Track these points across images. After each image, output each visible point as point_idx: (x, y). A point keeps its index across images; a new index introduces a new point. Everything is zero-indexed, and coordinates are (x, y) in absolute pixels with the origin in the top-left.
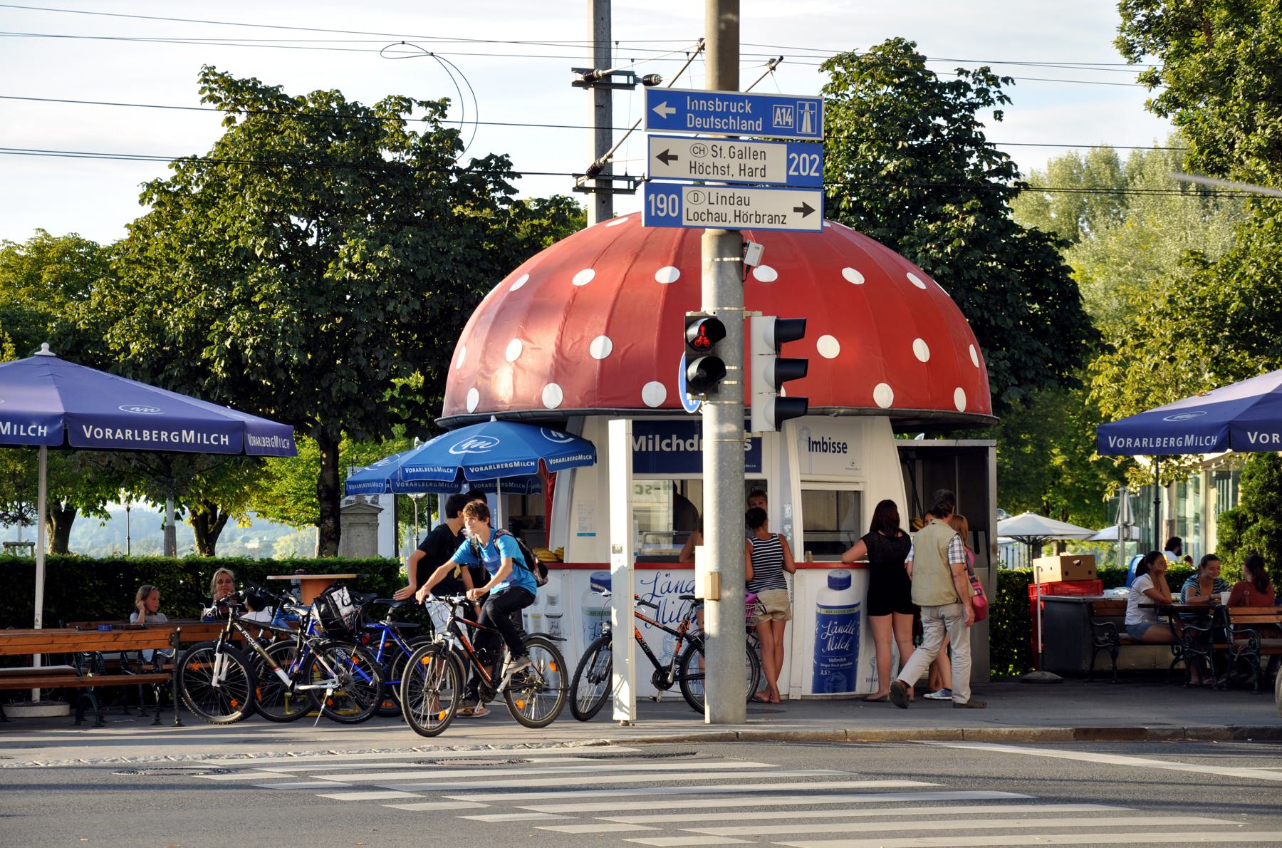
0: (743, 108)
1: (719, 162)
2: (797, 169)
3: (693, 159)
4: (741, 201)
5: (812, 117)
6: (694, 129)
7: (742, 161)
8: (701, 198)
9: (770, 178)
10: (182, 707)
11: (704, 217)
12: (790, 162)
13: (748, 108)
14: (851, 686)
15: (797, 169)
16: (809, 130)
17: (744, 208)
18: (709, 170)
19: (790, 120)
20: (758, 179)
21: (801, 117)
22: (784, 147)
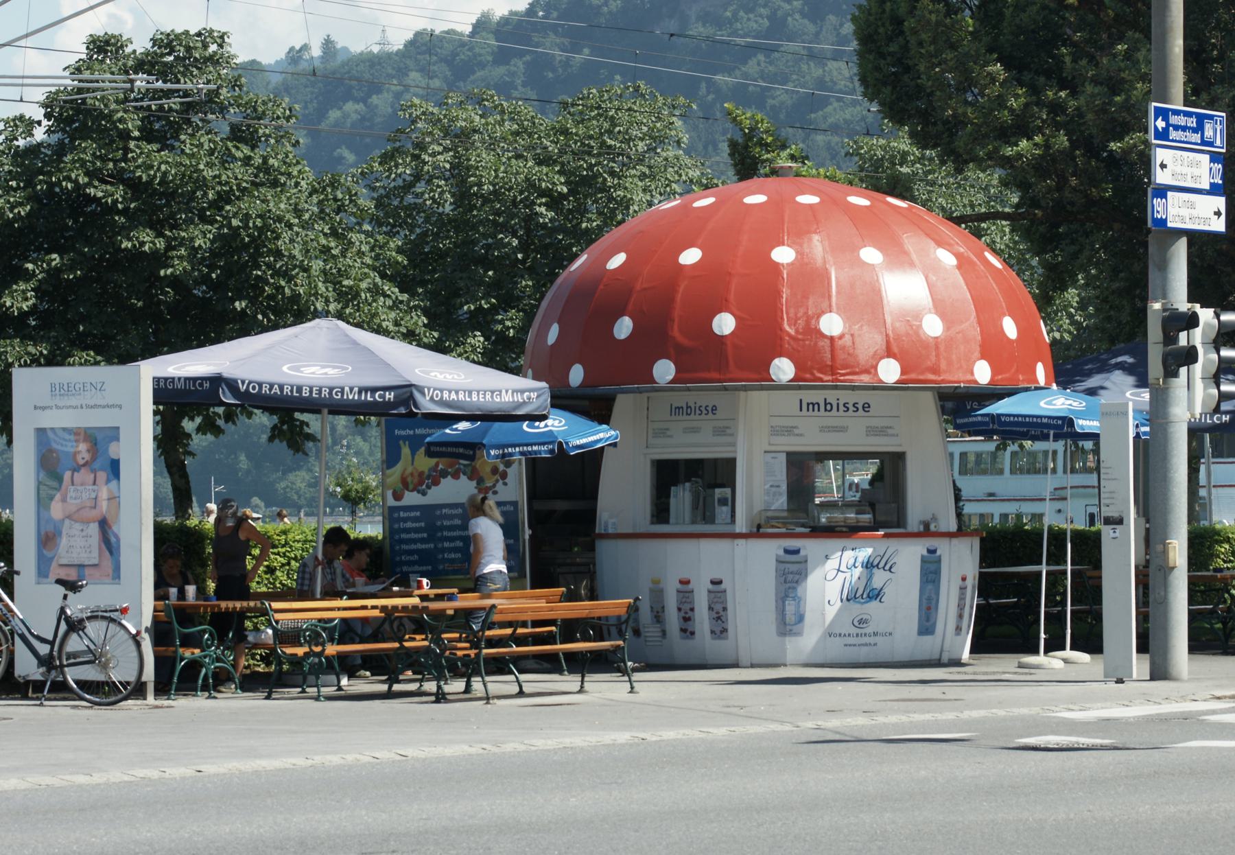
22: (1207, 157)
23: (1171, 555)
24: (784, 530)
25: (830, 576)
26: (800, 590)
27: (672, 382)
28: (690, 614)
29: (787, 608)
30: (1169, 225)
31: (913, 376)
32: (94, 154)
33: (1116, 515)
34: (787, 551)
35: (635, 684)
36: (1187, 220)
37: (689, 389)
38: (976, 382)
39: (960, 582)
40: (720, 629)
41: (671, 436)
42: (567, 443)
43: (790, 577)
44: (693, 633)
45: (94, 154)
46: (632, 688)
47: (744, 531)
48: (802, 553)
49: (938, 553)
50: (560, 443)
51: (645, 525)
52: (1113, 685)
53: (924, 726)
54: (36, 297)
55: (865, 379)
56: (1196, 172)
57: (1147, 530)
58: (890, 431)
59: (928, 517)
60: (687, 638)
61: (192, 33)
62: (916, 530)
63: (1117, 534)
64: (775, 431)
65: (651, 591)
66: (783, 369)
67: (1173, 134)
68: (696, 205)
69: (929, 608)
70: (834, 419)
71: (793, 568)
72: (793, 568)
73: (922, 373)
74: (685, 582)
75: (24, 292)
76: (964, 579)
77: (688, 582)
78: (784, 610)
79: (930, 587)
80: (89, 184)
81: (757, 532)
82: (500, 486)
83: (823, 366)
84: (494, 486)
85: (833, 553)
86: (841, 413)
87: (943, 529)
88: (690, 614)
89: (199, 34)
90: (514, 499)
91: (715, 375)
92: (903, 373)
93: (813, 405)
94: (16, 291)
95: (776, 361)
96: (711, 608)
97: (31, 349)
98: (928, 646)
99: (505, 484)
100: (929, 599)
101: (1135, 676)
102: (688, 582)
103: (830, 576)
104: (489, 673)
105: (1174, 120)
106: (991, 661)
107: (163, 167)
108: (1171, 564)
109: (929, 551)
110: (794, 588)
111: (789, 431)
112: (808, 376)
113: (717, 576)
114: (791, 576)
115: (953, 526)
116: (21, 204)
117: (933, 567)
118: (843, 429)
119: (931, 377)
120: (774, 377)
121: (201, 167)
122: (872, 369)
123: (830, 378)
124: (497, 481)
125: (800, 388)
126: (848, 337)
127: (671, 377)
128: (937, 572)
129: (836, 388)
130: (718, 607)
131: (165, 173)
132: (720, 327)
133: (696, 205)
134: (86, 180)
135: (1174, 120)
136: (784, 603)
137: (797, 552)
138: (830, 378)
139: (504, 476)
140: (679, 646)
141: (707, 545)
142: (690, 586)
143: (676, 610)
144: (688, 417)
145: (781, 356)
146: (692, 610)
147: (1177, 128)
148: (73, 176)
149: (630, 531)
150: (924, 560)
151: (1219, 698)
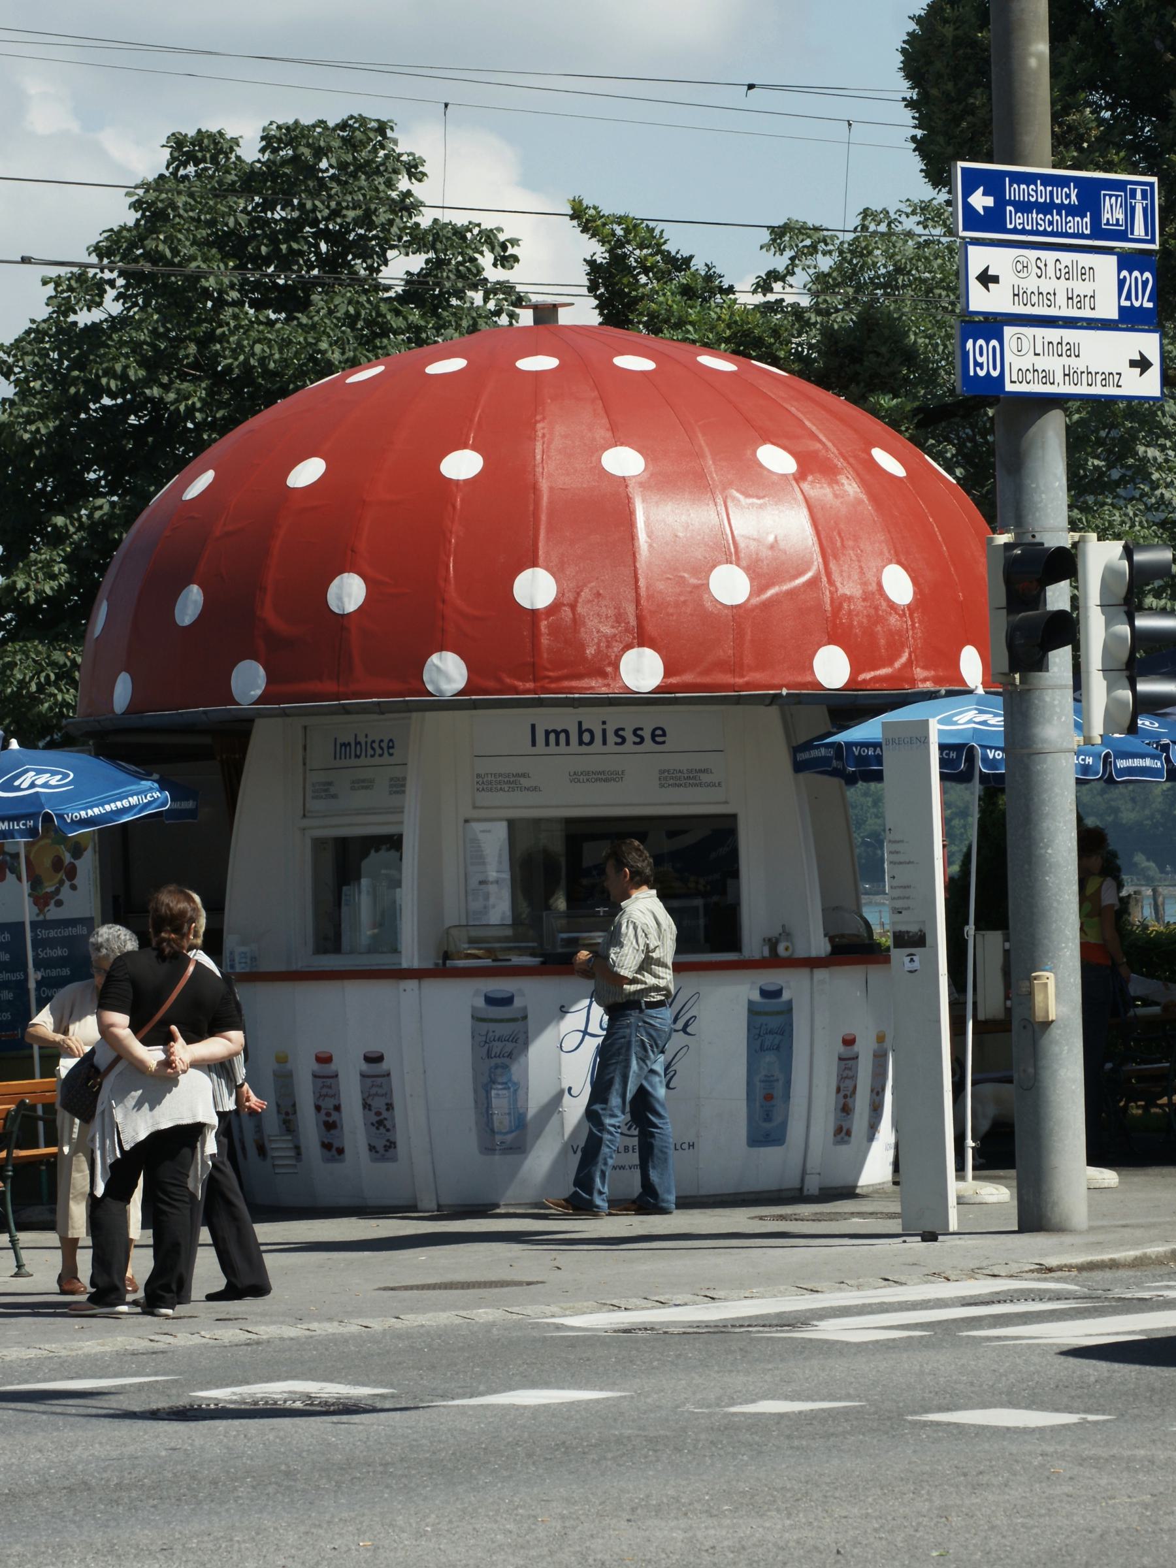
0: (1068, 196)
1: (1046, 286)
2: (1128, 298)
3: (1017, 281)
4: (1072, 351)
5: (1145, 210)
6: (1015, 231)
7: (1070, 284)
8: (1026, 345)
9: (1097, 314)
10: (369, 360)
11: (1030, 376)
12: (1121, 283)
13: (1073, 197)
14: (734, 943)
15: (1128, 298)
16: (1143, 233)
17: (1073, 362)
18: (1034, 299)
19: (1121, 217)
20: (1086, 313)
21: (1133, 209)
22: (1113, 260)
23: (1038, 998)
24: (488, 962)
25: (569, 1044)
26: (515, 1068)
27: (261, 700)
28: (334, 1116)
29: (494, 1102)
30: (1009, 387)
31: (688, 678)
32: (155, 330)
33: (913, 928)
34: (491, 1001)
35: (24, 1254)
36: (1059, 377)
37: (346, 710)
38: (819, 686)
39: (840, 1048)
40: (384, 1147)
41: (334, 796)
42: (61, 817)
43: (497, 1047)
44: (341, 1151)
45: (154, 332)
46: (20, 1266)
47: (416, 965)
48: (518, 1002)
49: (786, 996)
50: (48, 818)
51: (307, 960)
52: (915, 1244)
53: (34, 1369)
54: (69, 571)
55: (597, 687)
56: (1081, 288)
57: (1007, 953)
58: (705, 778)
59: (775, 932)
60: (332, 1160)
61: (331, 124)
62: (757, 956)
63: (916, 965)
64: (485, 783)
65: (277, 1075)
66: (448, 672)
67: (1015, 219)
68: (349, 381)
69: (769, 1097)
70: (598, 758)
71: (503, 1030)
72: (503, 1030)
73: (707, 672)
74: (374, 1059)
75: (49, 563)
76: (849, 1042)
77: (379, 1059)
78: (489, 1106)
79: (769, 1057)
80: (150, 381)
81: (444, 967)
82: (65, 893)
83: (527, 666)
84: (57, 891)
85: (576, 1001)
86: (611, 746)
87: (801, 953)
88: (334, 1116)
89: (343, 126)
90: (88, 915)
91: (330, 686)
92: (667, 673)
93: (556, 735)
94: (36, 562)
95: (435, 659)
96: (366, 1106)
97: (58, 657)
98: (772, 1165)
99: (74, 887)
100: (769, 1081)
101: (953, 1226)
102: (379, 1059)
103: (569, 1044)
104: (22, 1227)
105: (1016, 192)
106: (1136, 1179)
107: (258, 348)
108: (1039, 1016)
109: (764, 993)
110: (506, 1067)
111: (513, 782)
112: (491, 684)
113: (374, 1047)
114: (501, 1042)
115: (820, 946)
116: (42, 417)
117: (774, 1022)
118: (613, 777)
119: (728, 679)
120: (430, 688)
121: (324, 345)
122: (607, 667)
123: (530, 685)
124: (61, 883)
125: (475, 705)
126: (566, 613)
127: (259, 692)
128: (786, 1032)
129: (540, 703)
130: (328, 1104)
131: (263, 360)
132: (340, 599)
133: (349, 381)
134: (142, 373)
135: (1016, 192)
136: (488, 1093)
137: (508, 1001)
138: (530, 685)
139: (72, 873)
140: (324, 1176)
141: (356, 994)
142: (333, 1067)
143: (312, 1110)
144: (357, 762)
145: (441, 648)
146: (337, 1108)
147: (1024, 207)
148: (118, 367)
149: (281, 967)
150: (753, 1010)
151: (1050, 1270)
